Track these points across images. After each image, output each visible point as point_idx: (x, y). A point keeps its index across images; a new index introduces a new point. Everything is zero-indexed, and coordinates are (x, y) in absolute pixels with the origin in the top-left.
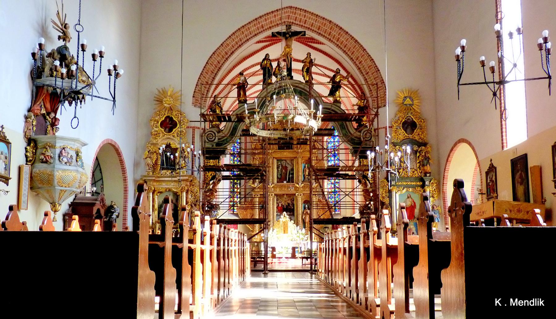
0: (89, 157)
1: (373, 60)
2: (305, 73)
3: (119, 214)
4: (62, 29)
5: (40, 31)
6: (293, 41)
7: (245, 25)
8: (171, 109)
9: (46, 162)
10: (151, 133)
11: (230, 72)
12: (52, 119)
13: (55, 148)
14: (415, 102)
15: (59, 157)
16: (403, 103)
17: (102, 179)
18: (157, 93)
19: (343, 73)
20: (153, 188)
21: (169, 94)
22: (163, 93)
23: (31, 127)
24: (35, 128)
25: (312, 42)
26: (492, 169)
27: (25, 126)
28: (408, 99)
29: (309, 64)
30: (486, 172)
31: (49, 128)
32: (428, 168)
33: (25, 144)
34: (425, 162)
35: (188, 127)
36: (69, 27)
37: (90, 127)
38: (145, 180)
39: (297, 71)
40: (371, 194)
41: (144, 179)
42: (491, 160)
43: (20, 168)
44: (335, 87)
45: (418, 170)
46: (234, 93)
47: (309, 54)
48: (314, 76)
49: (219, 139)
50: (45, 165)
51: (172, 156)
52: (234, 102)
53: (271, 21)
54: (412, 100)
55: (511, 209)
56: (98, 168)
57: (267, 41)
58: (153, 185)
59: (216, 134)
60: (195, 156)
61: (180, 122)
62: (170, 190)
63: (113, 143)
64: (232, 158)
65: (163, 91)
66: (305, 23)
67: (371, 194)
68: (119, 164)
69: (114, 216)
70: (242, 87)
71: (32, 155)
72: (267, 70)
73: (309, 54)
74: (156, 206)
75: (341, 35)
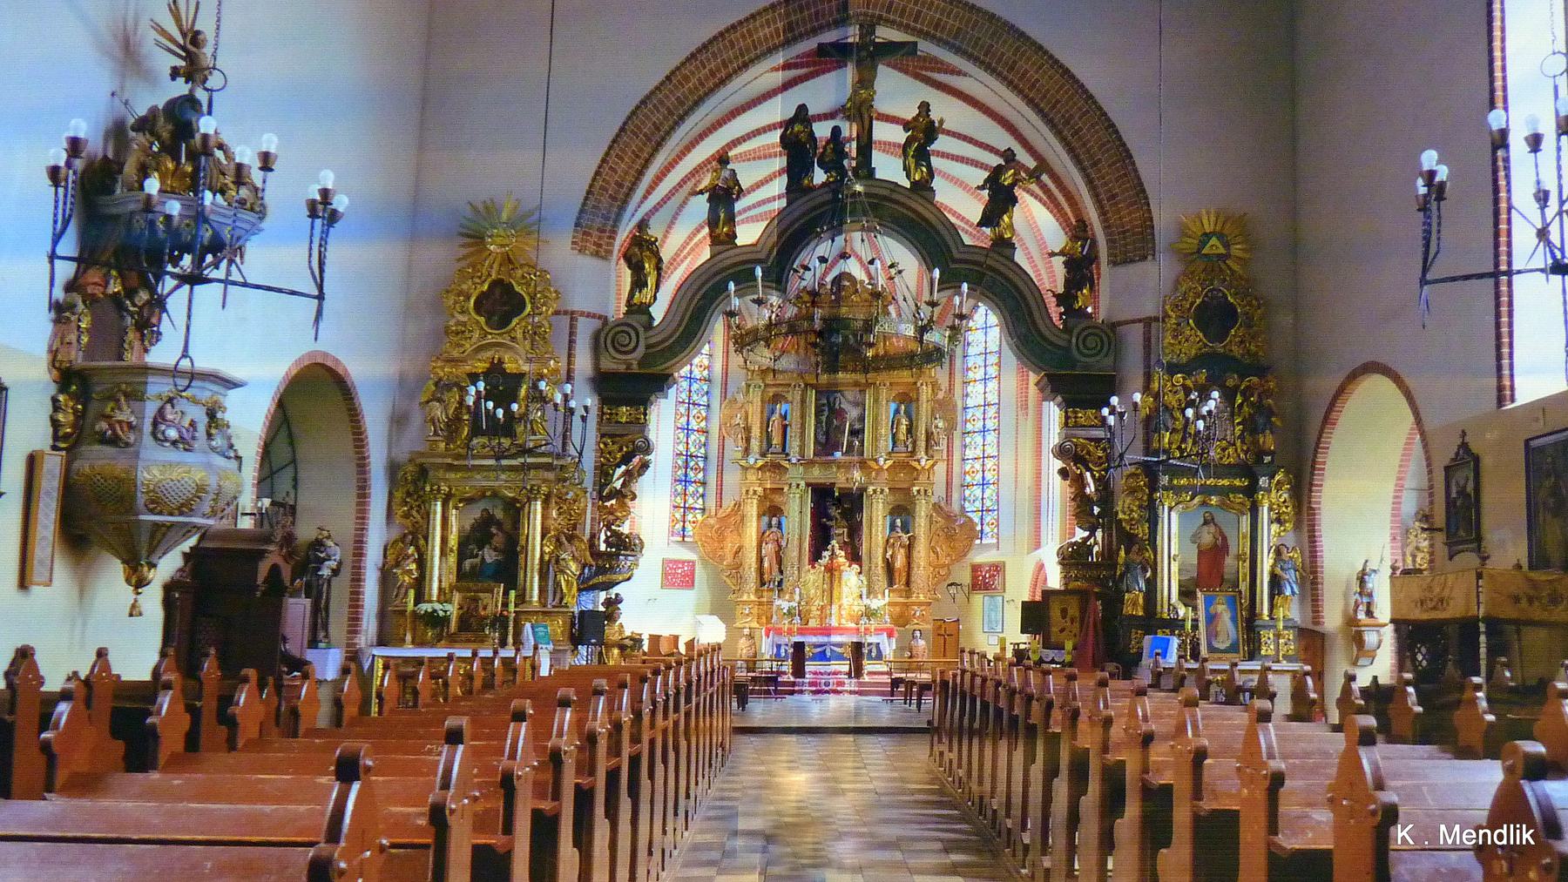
0: (248, 417)
1: (1113, 125)
2: (911, 161)
3: (340, 563)
4: (183, 48)
5: (119, 53)
6: (880, 67)
7: (741, 23)
8: (508, 260)
9: (114, 441)
10: (447, 327)
11: (702, 136)
12: (141, 308)
13: (142, 400)
14: (1236, 250)
15: (155, 424)
16: (1199, 251)
17: (294, 461)
18: (468, 211)
19: (1023, 157)
20: (445, 488)
21: (504, 216)
22: (489, 211)
23: (73, 337)
24: (85, 339)
25: (927, 69)
26: (1466, 460)
27: (55, 335)
28: (1214, 241)
29: (923, 133)
30: (1447, 469)
31: (132, 336)
32: (1268, 441)
33: (53, 389)
34: (1261, 421)
35: (557, 313)
36: (205, 40)
37: (234, 339)
38: (421, 465)
39: (887, 147)
40: (1096, 510)
41: (419, 461)
42: (1464, 434)
43: (32, 462)
44: (1000, 200)
45: (1238, 443)
46: (700, 205)
47: (925, 107)
48: (935, 161)
49: (648, 347)
50: (109, 450)
51: (500, 413)
52: (698, 230)
53: (817, 13)
54: (1227, 245)
55: (1532, 592)
56: (283, 434)
57: (807, 65)
58: (446, 480)
59: (641, 330)
60: (572, 411)
61: (533, 298)
62: (495, 494)
63: (329, 364)
64: (682, 436)
65: (487, 208)
66: (916, 21)
67: (1096, 510)
68: (347, 419)
69: (325, 572)
70: (724, 197)
71: (71, 418)
72: (797, 145)
73: (925, 107)
74: (453, 541)
75: (1023, 55)
